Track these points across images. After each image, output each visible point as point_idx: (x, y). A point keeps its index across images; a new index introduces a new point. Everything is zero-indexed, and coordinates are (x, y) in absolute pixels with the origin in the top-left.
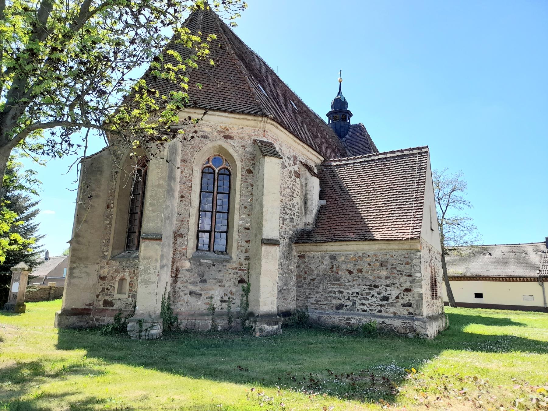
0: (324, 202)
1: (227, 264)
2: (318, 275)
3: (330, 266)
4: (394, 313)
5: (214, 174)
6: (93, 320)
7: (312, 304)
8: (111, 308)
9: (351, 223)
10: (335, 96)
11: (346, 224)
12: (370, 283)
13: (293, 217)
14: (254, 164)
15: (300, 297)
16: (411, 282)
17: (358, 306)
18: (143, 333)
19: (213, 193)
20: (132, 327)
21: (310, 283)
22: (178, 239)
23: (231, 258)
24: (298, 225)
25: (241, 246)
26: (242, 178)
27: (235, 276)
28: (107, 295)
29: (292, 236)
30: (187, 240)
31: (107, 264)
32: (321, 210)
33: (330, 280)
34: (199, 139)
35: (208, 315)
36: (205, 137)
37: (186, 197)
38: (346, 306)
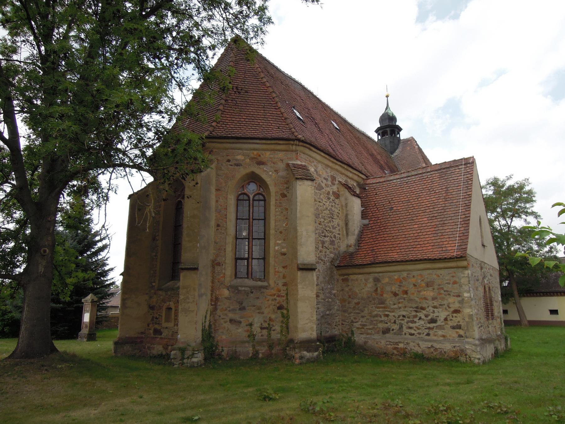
0: (366, 222)
1: (264, 290)
2: (363, 299)
3: (375, 289)
4: (444, 336)
5: (249, 200)
6: (145, 348)
7: (358, 328)
8: (160, 336)
9: (395, 243)
10: (382, 111)
11: (389, 244)
12: (416, 305)
13: (334, 239)
14: (288, 188)
15: (345, 321)
16: (459, 302)
17: (405, 330)
18: (185, 361)
19: (249, 219)
20: (175, 354)
21: (354, 307)
22: (216, 267)
23: (269, 284)
24: (339, 247)
25: (278, 272)
26: (276, 203)
27: (273, 302)
28: (156, 323)
29: (333, 259)
30: (225, 269)
31: (155, 293)
32: (364, 228)
33: (374, 304)
34: (233, 167)
35: (248, 342)
36: (237, 165)
37: (221, 225)
38: (393, 330)
